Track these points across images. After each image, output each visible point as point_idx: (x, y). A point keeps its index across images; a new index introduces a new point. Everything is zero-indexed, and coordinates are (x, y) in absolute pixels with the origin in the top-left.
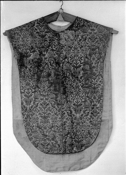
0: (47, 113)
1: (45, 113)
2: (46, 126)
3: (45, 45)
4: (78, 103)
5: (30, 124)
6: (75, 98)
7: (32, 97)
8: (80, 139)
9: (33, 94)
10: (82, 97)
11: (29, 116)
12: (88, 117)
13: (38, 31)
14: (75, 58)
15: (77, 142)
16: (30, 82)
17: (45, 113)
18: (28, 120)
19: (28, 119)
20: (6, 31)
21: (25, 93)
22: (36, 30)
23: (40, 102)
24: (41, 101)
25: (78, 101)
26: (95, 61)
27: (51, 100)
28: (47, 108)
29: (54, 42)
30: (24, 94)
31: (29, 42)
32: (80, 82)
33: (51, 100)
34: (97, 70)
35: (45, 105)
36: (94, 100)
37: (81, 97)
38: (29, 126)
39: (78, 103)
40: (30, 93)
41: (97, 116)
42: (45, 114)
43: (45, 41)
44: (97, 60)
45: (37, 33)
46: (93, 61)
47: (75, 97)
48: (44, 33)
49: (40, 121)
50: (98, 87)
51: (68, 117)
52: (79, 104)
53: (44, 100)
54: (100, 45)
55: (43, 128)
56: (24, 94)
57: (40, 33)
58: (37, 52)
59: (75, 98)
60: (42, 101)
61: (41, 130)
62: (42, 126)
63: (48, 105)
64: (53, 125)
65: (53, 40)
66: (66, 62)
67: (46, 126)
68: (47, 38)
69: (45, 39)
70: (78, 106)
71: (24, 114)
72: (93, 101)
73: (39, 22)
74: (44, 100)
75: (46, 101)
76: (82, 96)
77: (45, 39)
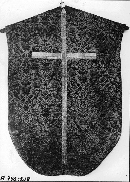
0: (48, 105)
1: (46, 105)
2: (46, 27)
3: (47, 27)
4: (83, 70)
5: (28, 117)
6: (80, 20)
7: (31, 85)
8: (83, 26)
9: (32, 81)
10: (89, 107)
11: (28, 109)
12: (94, 42)
13: (41, 103)
14: (82, 63)
15: (81, 116)
16: (29, 116)
17: (46, 105)
18: (26, 67)
19: (26, 112)
20: (6, 27)
21: (22, 35)
22: (39, 102)
23: (41, 47)
24: (42, 47)
25: (82, 23)
26: (104, 65)
27: (53, 46)
28: (49, 98)
29: (57, 25)
30: (21, 37)
31: (30, 115)
32: (86, 90)
33: (53, 46)
34: (105, 31)
35: (46, 95)
36: (102, 65)
37: (87, 107)
38: (27, 28)
39: (83, 70)
40: (28, 36)
41: (105, 84)
42: (47, 61)
43: (48, 70)
44: (106, 151)
45: (40, 105)
46: (102, 65)
47: (79, 18)
48: (48, 61)
49: (40, 114)
50: (106, 94)
51: (71, 44)
52: (84, 71)
53: (45, 45)
54: (111, 90)
55: (43, 123)
56: (21, 37)
57: (44, 61)
58: (38, 37)
59: (80, 20)
60: (43, 47)
61: (41, 78)
62: (43, 119)
63: (50, 95)
64: (55, 118)
65: (57, 23)
66: (72, 68)
67: (46, 27)
68: (51, 112)
69: (49, 68)
70: (83, 74)
71: (21, 105)
72: (101, 67)
73: (43, 94)
74: (45, 45)
75: (48, 47)
76: (87, 17)
77: (49, 68)
